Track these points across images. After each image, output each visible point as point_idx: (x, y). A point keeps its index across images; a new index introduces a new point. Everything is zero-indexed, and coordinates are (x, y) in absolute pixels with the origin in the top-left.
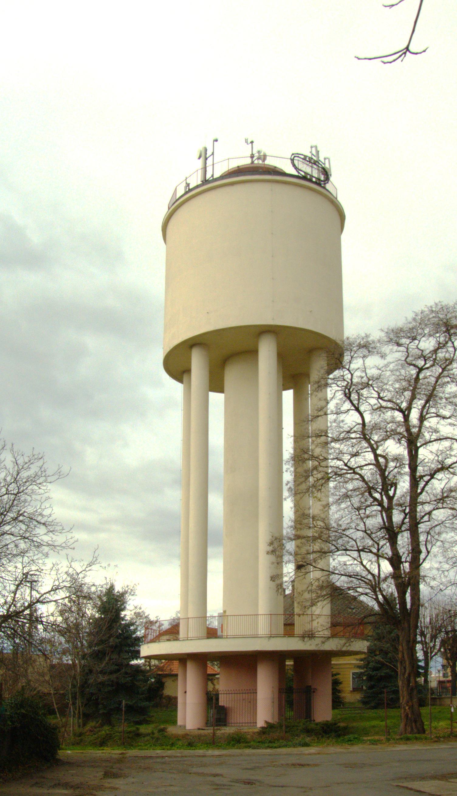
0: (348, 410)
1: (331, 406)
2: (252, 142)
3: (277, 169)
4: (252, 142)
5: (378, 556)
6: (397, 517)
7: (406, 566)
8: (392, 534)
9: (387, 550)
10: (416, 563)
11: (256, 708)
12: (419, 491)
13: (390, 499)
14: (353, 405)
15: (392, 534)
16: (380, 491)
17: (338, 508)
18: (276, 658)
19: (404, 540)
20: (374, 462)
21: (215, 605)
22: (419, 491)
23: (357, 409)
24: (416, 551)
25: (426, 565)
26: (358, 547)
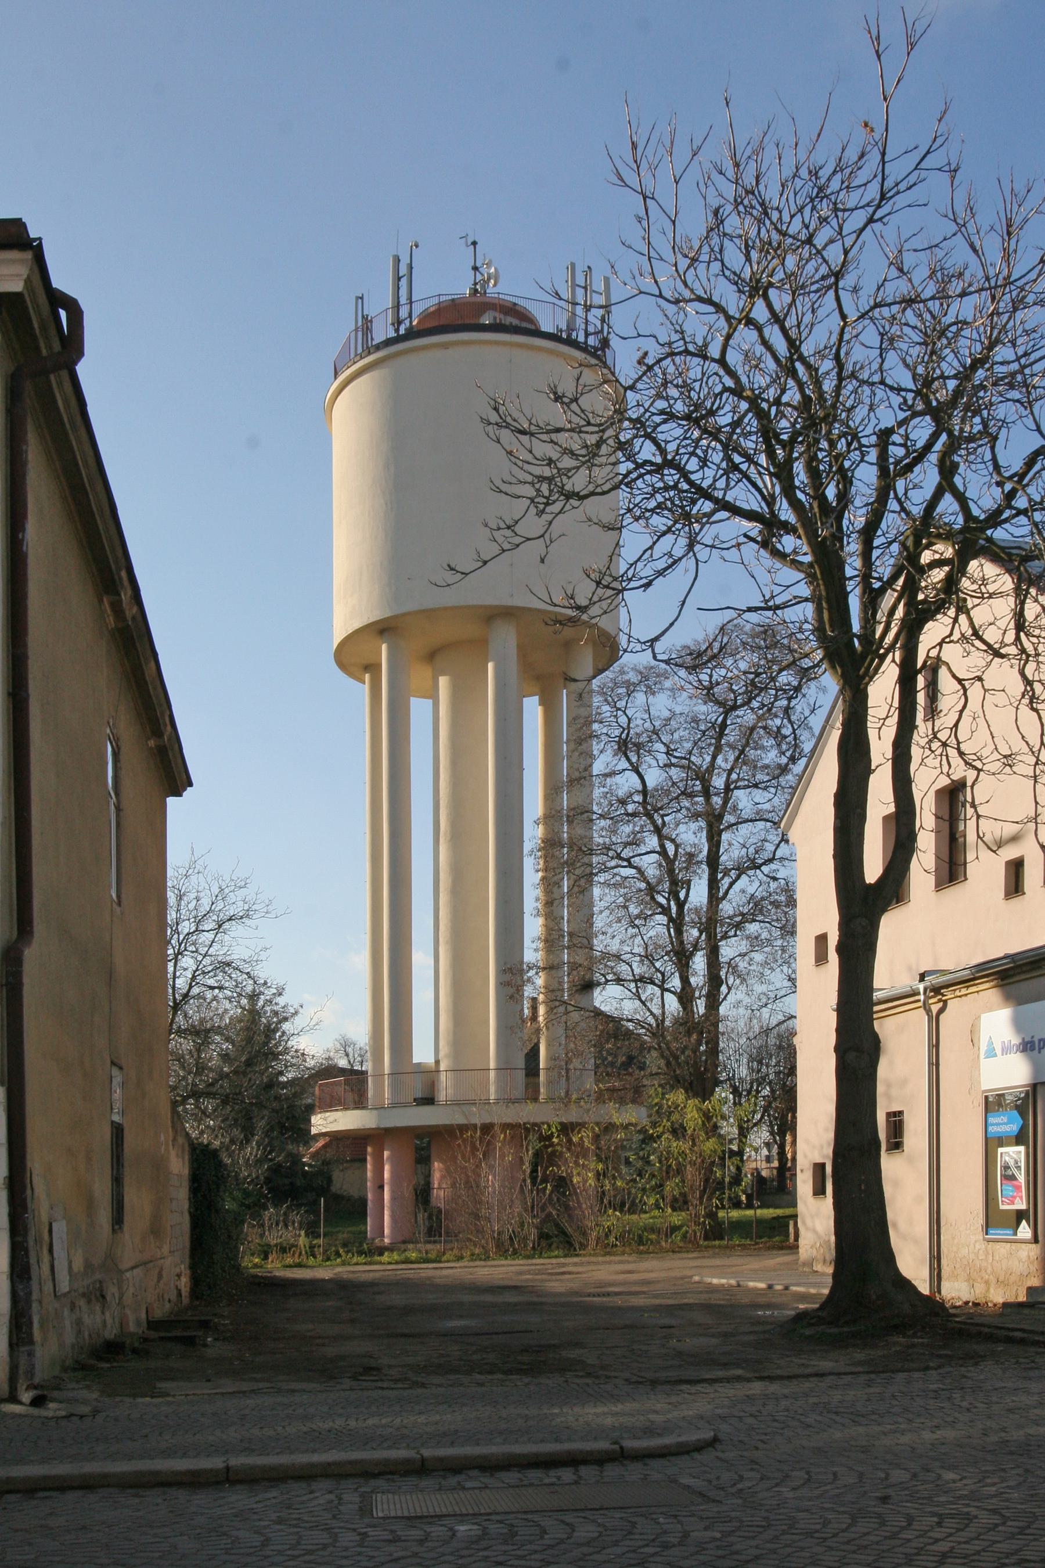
0: (624, 770)
1: (598, 767)
2: (474, 243)
3: (517, 308)
4: (474, 243)
5: (664, 990)
6: (692, 933)
7: (700, 1007)
8: (682, 958)
9: (676, 983)
10: (714, 1001)
11: (122, 1141)
12: (721, 894)
13: (681, 905)
14: (631, 764)
15: (682, 958)
16: (667, 895)
17: (940, 253)
18: (520, 1131)
19: (699, 962)
20: (658, 849)
21: (423, 1053)
22: (721, 894)
23: (636, 770)
24: (714, 980)
25: (723, 1010)
26: (634, 975)
